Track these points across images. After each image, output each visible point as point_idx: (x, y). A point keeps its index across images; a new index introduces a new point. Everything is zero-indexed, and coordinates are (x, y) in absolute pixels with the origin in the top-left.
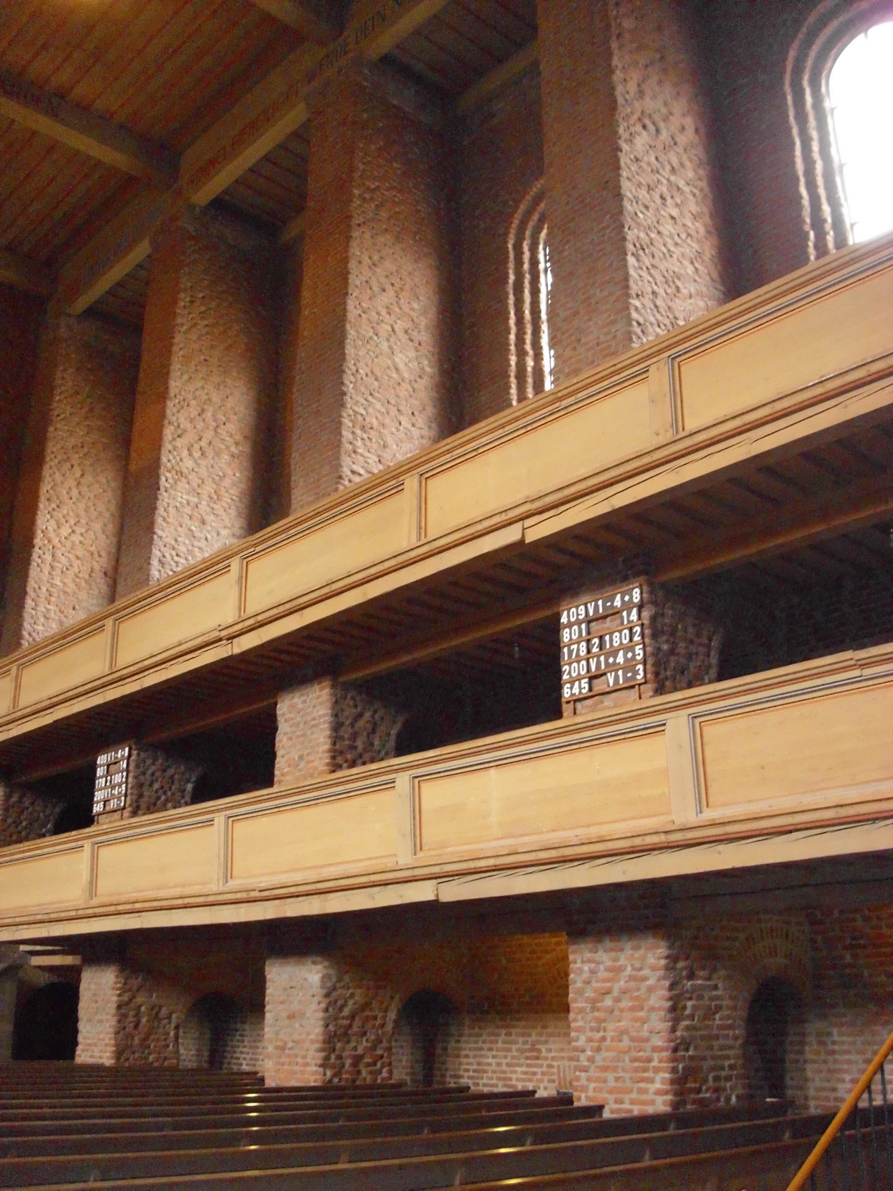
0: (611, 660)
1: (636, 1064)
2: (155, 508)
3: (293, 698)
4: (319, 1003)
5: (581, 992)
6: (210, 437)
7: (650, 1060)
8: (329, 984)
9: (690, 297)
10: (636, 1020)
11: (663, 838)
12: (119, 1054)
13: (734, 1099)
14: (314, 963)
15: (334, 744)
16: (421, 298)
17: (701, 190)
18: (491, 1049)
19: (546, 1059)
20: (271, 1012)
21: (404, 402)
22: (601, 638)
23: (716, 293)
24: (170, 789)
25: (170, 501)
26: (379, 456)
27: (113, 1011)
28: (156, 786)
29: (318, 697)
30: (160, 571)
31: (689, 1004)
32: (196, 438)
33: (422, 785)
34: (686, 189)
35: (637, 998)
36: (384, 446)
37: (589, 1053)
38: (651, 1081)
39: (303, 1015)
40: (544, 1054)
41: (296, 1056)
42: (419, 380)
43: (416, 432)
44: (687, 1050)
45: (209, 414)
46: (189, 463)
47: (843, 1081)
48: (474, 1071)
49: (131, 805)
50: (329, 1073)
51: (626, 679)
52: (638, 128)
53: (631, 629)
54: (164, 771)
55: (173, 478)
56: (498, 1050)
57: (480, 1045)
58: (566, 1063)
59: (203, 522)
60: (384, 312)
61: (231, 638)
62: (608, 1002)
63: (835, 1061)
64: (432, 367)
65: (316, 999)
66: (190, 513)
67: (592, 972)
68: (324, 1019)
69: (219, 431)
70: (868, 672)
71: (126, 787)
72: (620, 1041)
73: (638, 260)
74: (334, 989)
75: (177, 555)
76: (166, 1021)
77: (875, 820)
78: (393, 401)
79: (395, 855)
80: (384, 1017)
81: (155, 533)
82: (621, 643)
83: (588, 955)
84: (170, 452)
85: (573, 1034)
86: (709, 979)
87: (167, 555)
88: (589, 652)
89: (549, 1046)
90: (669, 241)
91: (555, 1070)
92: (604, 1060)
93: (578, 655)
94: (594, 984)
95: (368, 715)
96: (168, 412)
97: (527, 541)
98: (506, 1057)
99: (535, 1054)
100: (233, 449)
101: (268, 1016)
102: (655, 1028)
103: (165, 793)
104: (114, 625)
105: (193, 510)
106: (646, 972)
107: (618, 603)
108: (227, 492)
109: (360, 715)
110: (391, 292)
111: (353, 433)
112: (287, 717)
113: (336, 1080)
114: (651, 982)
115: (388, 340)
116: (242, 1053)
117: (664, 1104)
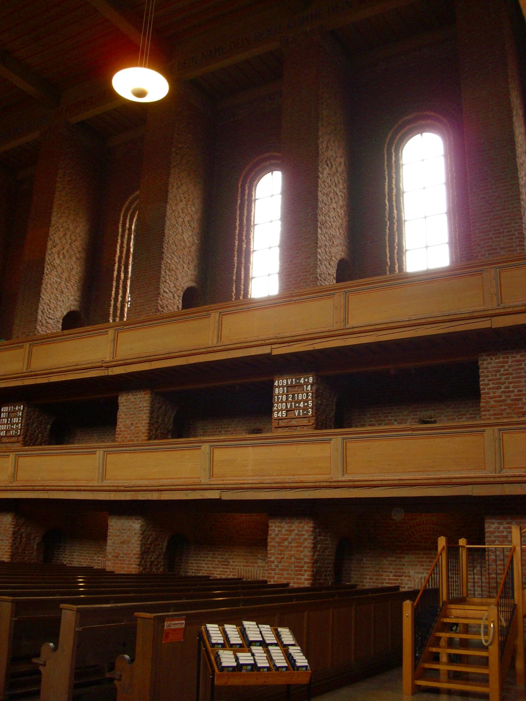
0: (297, 405)
1: (297, 568)
2: (41, 284)
3: (128, 396)
4: (139, 537)
5: (273, 539)
6: (68, 248)
7: (303, 567)
8: (143, 529)
9: (337, 246)
10: (298, 551)
11: (328, 484)
12: (12, 556)
13: (330, 584)
14: (136, 519)
15: (150, 420)
16: (196, 205)
17: (344, 194)
18: (204, 561)
19: (232, 565)
20: (111, 540)
21: (185, 257)
22: (293, 395)
23: (346, 243)
24: (40, 427)
25: (49, 281)
26: (174, 284)
27: (11, 535)
28: (35, 425)
29: (143, 398)
30: (42, 317)
31: (319, 546)
32: (62, 248)
33: (215, 450)
34: (339, 194)
35: (300, 542)
36: (177, 279)
37: (276, 563)
38: (303, 575)
39: (129, 542)
40: (231, 563)
41: (124, 560)
42: (192, 247)
43: (190, 272)
44: (317, 564)
45: (68, 237)
46: (58, 261)
47: (366, 578)
48: (195, 570)
49: (23, 434)
50: (141, 569)
51: (304, 414)
52: (326, 166)
53: (307, 394)
54: (38, 418)
55: (50, 268)
56: (208, 561)
57: (199, 558)
58: (243, 568)
59: (62, 292)
60: (180, 211)
61: (108, 367)
62: (286, 543)
63: (364, 571)
64: (197, 240)
65: (138, 535)
66: (56, 287)
67: (279, 531)
68: (140, 544)
69: (72, 245)
70: (414, 433)
71: (21, 425)
72: (291, 559)
73: (321, 230)
74: (145, 531)
75: (50, 309)
76: (32, 541)
77: (412, 486)
78: (182, 257)
79: (199, 478)
80: (162, 545)
81: (41, 297)
82: (302, 398)
83: (278, 524)
84: (50, 254)
85: (269, 556)
86: (325, 536)
87: (45, 308)
88: (287, 399)
89: (234, 560)
90: (332, 220)
91: (237, 571)
92: (283, 566)
93: (282, 400)
94: (280, 536)
95: (164, 407)
96: (50, 234)
97: (273, 354)
98: (212, 564)
99: (226, 563)
100: (78, 255)
101: (109, 542)
102: (306, 555)
103: (38, 429)
104: (30, 347)
105: (58, 286)
106: (304, 532)
107: (302, 381)
108: (73, 277)
109: (161, 407)
110: (184, 202)
111: (165, 272)
112: (125, 404)
113: (144, 572)
114: (306, 536)
115: (182, 226)
116: (63, 557)
117: (308, 584)
